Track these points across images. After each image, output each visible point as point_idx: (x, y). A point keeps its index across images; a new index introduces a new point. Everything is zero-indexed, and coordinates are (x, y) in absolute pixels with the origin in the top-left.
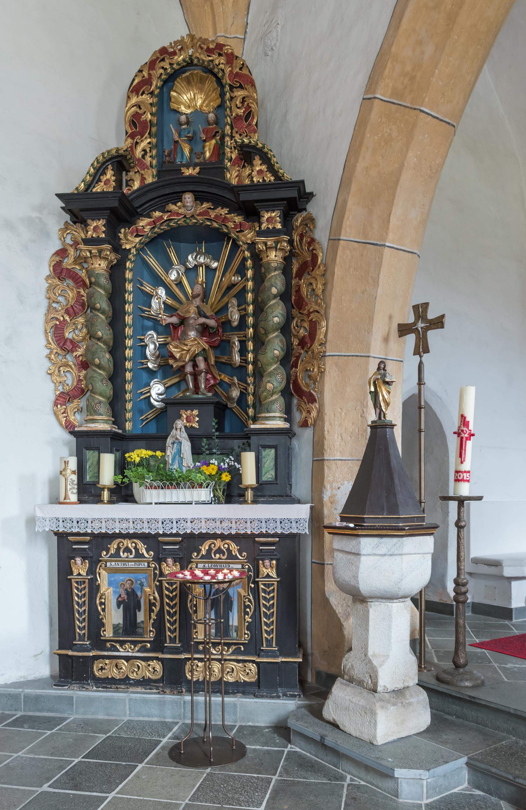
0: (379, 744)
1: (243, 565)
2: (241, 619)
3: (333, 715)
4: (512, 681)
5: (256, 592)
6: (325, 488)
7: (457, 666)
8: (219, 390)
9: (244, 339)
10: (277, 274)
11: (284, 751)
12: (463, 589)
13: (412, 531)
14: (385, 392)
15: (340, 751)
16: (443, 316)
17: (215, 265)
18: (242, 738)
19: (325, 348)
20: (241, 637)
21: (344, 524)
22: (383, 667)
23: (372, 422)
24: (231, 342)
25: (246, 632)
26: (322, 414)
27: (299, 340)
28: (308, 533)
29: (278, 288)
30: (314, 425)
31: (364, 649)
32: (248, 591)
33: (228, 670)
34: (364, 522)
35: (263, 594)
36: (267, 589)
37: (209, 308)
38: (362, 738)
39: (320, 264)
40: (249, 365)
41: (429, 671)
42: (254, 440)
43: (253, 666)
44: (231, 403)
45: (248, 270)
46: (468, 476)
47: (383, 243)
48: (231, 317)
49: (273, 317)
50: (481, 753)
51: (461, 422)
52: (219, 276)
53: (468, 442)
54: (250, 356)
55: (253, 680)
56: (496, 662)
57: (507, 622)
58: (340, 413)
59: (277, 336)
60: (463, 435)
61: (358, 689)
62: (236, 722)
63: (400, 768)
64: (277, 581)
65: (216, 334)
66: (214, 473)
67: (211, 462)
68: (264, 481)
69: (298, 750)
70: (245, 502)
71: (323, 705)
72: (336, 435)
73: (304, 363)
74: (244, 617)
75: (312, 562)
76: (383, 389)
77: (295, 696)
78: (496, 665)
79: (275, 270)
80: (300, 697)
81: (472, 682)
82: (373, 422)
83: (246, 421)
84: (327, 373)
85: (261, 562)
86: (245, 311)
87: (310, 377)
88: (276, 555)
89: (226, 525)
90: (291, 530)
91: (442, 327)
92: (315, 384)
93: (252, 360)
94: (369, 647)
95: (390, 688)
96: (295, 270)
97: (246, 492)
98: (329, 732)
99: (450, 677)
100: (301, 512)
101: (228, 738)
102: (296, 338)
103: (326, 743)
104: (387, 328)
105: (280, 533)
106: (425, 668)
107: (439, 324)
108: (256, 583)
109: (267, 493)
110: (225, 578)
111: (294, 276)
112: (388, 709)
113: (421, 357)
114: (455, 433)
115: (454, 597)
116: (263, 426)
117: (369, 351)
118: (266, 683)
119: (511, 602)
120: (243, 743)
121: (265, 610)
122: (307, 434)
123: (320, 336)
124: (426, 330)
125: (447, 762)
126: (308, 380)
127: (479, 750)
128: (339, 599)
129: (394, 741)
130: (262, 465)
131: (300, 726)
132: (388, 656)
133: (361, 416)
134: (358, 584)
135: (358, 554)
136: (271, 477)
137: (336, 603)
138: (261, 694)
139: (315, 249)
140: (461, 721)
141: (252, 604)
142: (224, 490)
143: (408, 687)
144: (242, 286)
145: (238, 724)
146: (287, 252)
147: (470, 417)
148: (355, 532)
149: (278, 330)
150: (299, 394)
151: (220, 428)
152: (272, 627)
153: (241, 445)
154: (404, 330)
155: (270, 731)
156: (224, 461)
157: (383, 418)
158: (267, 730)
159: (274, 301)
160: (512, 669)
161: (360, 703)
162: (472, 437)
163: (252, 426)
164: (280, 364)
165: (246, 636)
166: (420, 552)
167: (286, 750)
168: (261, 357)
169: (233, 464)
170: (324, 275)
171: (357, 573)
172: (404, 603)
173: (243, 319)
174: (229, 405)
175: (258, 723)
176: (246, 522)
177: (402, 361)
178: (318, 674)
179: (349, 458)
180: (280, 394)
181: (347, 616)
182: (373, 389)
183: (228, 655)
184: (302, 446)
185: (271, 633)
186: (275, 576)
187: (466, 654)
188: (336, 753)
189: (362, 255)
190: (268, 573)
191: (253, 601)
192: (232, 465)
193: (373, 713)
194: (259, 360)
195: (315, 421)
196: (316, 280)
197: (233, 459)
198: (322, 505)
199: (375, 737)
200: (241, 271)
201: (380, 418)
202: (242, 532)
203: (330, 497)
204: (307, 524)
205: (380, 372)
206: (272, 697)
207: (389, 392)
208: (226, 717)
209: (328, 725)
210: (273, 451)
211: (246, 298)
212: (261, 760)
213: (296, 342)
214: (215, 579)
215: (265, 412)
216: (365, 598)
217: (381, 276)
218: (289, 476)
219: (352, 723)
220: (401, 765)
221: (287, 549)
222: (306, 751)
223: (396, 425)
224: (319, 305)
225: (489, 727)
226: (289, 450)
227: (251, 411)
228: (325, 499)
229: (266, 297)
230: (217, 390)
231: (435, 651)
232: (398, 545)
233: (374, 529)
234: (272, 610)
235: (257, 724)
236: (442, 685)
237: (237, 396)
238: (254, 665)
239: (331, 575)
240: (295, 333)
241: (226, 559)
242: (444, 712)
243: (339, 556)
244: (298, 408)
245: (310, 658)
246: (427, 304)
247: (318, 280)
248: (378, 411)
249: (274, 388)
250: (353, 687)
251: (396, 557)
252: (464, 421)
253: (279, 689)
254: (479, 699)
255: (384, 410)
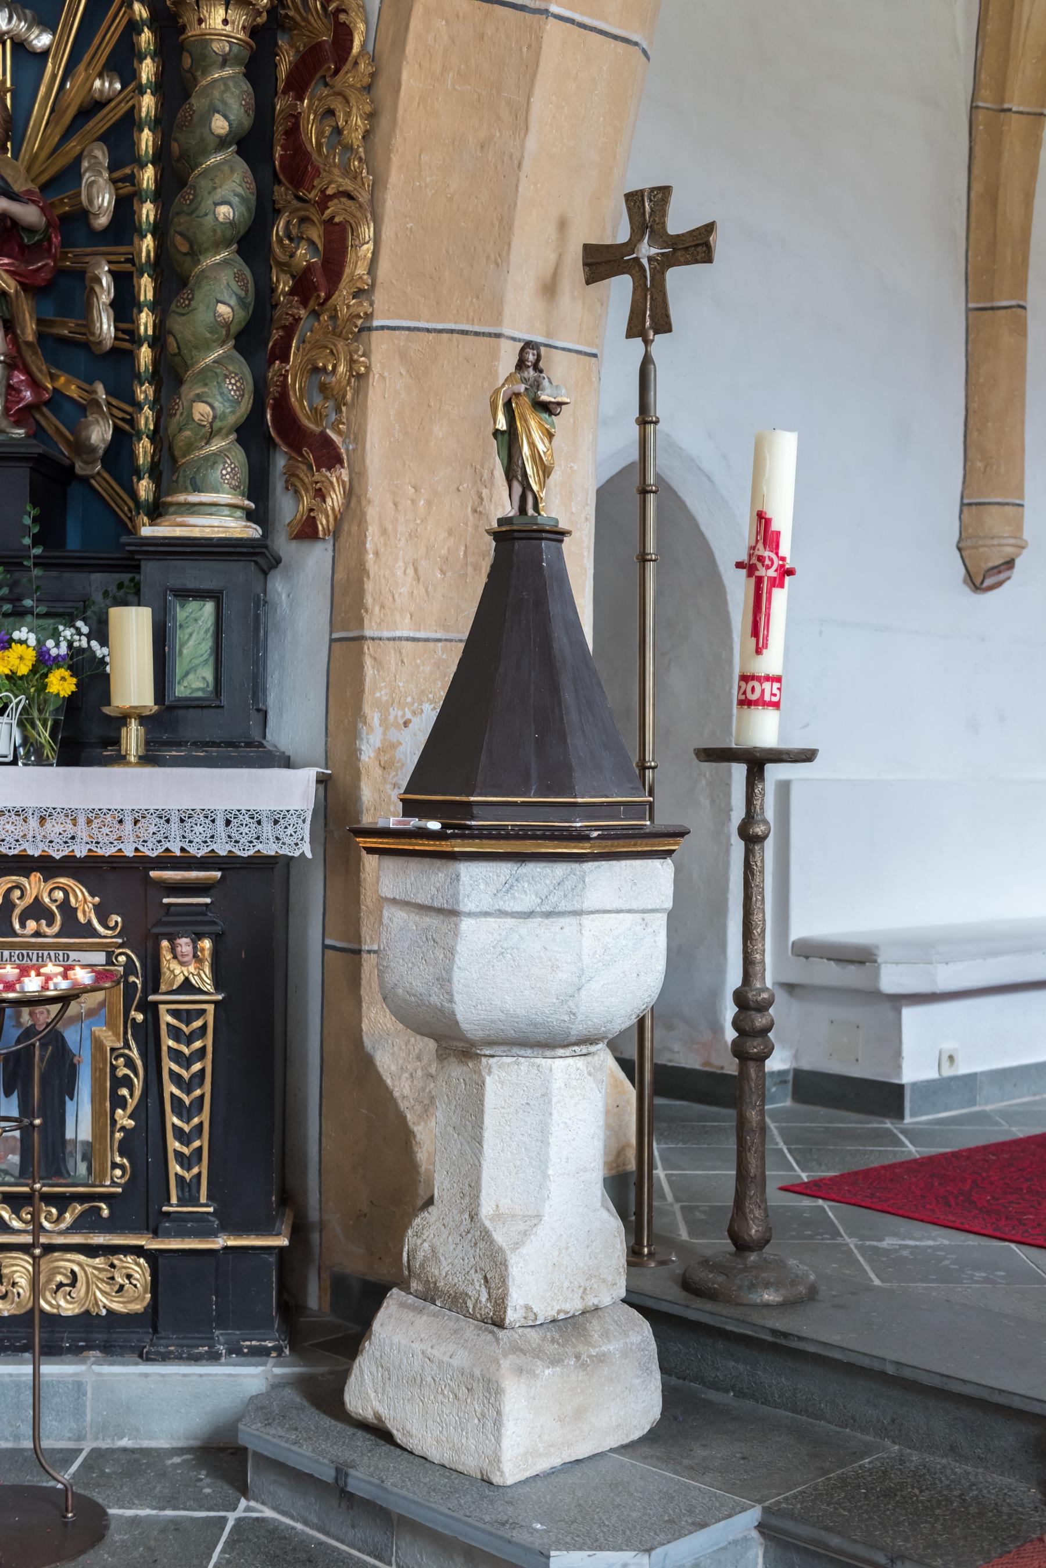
0: (510, 1482)
1: (109, 955)
2: (103, 1121)
3: (376, 1404)
4: (895, 1285)
5: (148, 1036)
6: (365, 723)
7: (742, 1245)
8: (49, 421)
9: (128, 267)
10: (230, 77)
11: (224, 1519)
12: (760, 1021)
13: (609, 843)
14: (537, 435)
15: (391, 1507)
16: (710, 228)
17: (42, 40)
18: (98, 1485)
19: (372, 304)
20: (102, 1175)
21: (414, 822)
22: (523, 1250)
23: (499, 520)
24: (89, 275)
25: (118, 1159)
26: (359, 502)
27: (293, 277)
28: (309, 855)
29: (232, 117)
30: (336, 534)
31: (467, 1199)
32: (125, 1033)
33: (59, 1278)
34: (472, 818)
35: (171, 1043)
36: (183, 1027)
37: (22, 169)
38: (460, 1468)
39: (360, 53)
40: (141, 345)
41: (662, 1263)
42: (150, 570)
43: (138, 1264)
44: (86, 463)
45: (141, 60)
46: (775, 691)
47: (543, 6)
48: (91, 202)
49: (216, 204)
50: (801, 1493)
51: (758, 533)
52: (54, 76)
53: (776, 591)
54: (145, 320)
55: (138, 1307)
56: (851, 1235)
57: (888, 1124)
58: (413, 501)
59: (225, 262)
60: (762, 572)
61: (450, 1319)
62: (80, 1438)
63: (568, 1549)
64: (215, 1003)
65: (41, 249)
66: (23, 670)
67: (16, 635)
68: (179, 699)
69: (268, 1513)
70: (120, 759)
71: (343, 1376)
72: (401, 564)
73: (308, 346)
74: (113, 1113)
75: (325, 947)
76: (533, 424)
77: (264, 1352)
78: (852, 1242)
79: (225, 62)
80: (279, 1355)
81: (783, 1291)
82: (501, 521)
83: (130, 519)
84: (374, 380)
85: (165, 943)
86: (133, 185)
87: (323, 388)
88: (214, 923)
89: (59, 828)
90: (259, 847)
91: (708, 259)
92: (338, 410)
93: (150, 332)
94: (484, 1192)
95: (545, 1311)
96: (283, 70)
97: (124, 731)
98: (363, 1455)
99: (721, 1279)
100: (293, 791)
101: (54, 1488)
102: (285, 272)
103: (354, 1486)
104: (553, 257)
105: (223, 853)
106: (650, 1254)
107: (699, 249)
108: (151, 1010)
109: (190, 733)
110: (48, 989)
111: (281, 85)
112: (535, 1376)
113: (647, 342)
114: (739, 565)
115: (734, 1041)
116: (178, 532)
117: (499, 322)
118: (176, 1317)
119: (900, 1067)
120: (100, 1501)
121: (177, 1092)
122: (315, 560)
123: (357, 267)
124: (663, 264)
125: (703, 1526)
126: (318, 400)
127: (796, 1485)
128: (403, 1054)
129: (553, 1472)
130: (174, 648)
131: (274, 1440)
132: (539, 1217)
133: (475, 511)
134: (451, 1001)
135: (452, 913)
136: (202, 685)
137: (393, 1068)
138: (162, 1349)
139: (344, 11)
140: (749, 1404)
141: (136, 1075)
142: (56, 723)
143: (597, 1309)
144: (124, 108)
145: (87, 1446)
146: (260, 14)
147: (783, 522)
148: (445, 846)
149: (229, 245)
150: (290, 440)
151: (49, 533)
152: (197, 1144)
153: (113, 588)
154: (601, 263)
155: (184, 1461)
156: (56, 635)
157: (531, 511)
158: (177, 1460)
159: (219, 157)
160: (896, 1251)
161: (455, 1362)
162: (787, 579)
163: (147, 531)
164: (236, 347)
165: (118, 1172)
166: (634, 906)
167: (232, 1517)
168: (176, 324)
169: (84, 644)
170: (368, 88)
171: (449, 971)
172: (589, 1058)
173: (125, 206)
174: (80, 468)
175: (151, 1438)
176: (121, 822)
177: (595, 356)
178: (339, 1285)
179: (439, 635)
180: (233, 437)
181: (428, 1105)
182: (502, 424)
183: (61, 1233)
184: (301, 595)
185: (194, 1160)
186: (209, 987)
187: (766, 1210)
188: (381, 1518)
189: (482, 36)
190: (187, 979)
191: (139, 1063)
192: (81, 650)
193: (492, 1391)
194: (170, 332)
195: (339, 521)
196: (347, 101)
197: (85, 630)
198: (357, 776)
199: (496, 1460)
200: (122, 62)
201: (523, 510)
202: (109, 851)
203: (380, 751)
204: (307, 826)
205: (526, 375)
206: (196, 1359)
207: (550, 436)
208: (48, 1422)
209: (360, 1433)
210: (209, 607)
211: (134, 145)
212: (150, 1549)
213: (284, 285)
214: (14, 991)
215: (185, 490)
216: (473, 1044)
217: (536, 101)
218: (256, 686)
219: (430, 1422)
220: (568, 1539)
221: (247, 909)
222: (292, 1518)
223: (569, 533)
224: (355, 177)
225: (826, 1420)
226: (257, 606)
227: (145, 488)
228: (364, 757)
229: (193, 142)
230: (43, 422)
231: (682, 1207)
232: (568, 885)
233: (498, 837)
234: (198, 1092)
235: (146, 1444)
236: (699, 1303)
237: (103, 439)
238: (142, 1261)
239: (375, 986)
240: (283, 258)
241: (57, 935)
242: (703, 1383)
243: (396, 919)
244: (287, 481)
245: (315, 1237)
246: (664, 192)
247: (353, 102)
248: (517, 489)
249: (215, 417)
250: (435, 1315)
251: (563, 921)
252: (766, 533)
253: (217, 1332)
254: (801, 1339)
255: (535, 488)
